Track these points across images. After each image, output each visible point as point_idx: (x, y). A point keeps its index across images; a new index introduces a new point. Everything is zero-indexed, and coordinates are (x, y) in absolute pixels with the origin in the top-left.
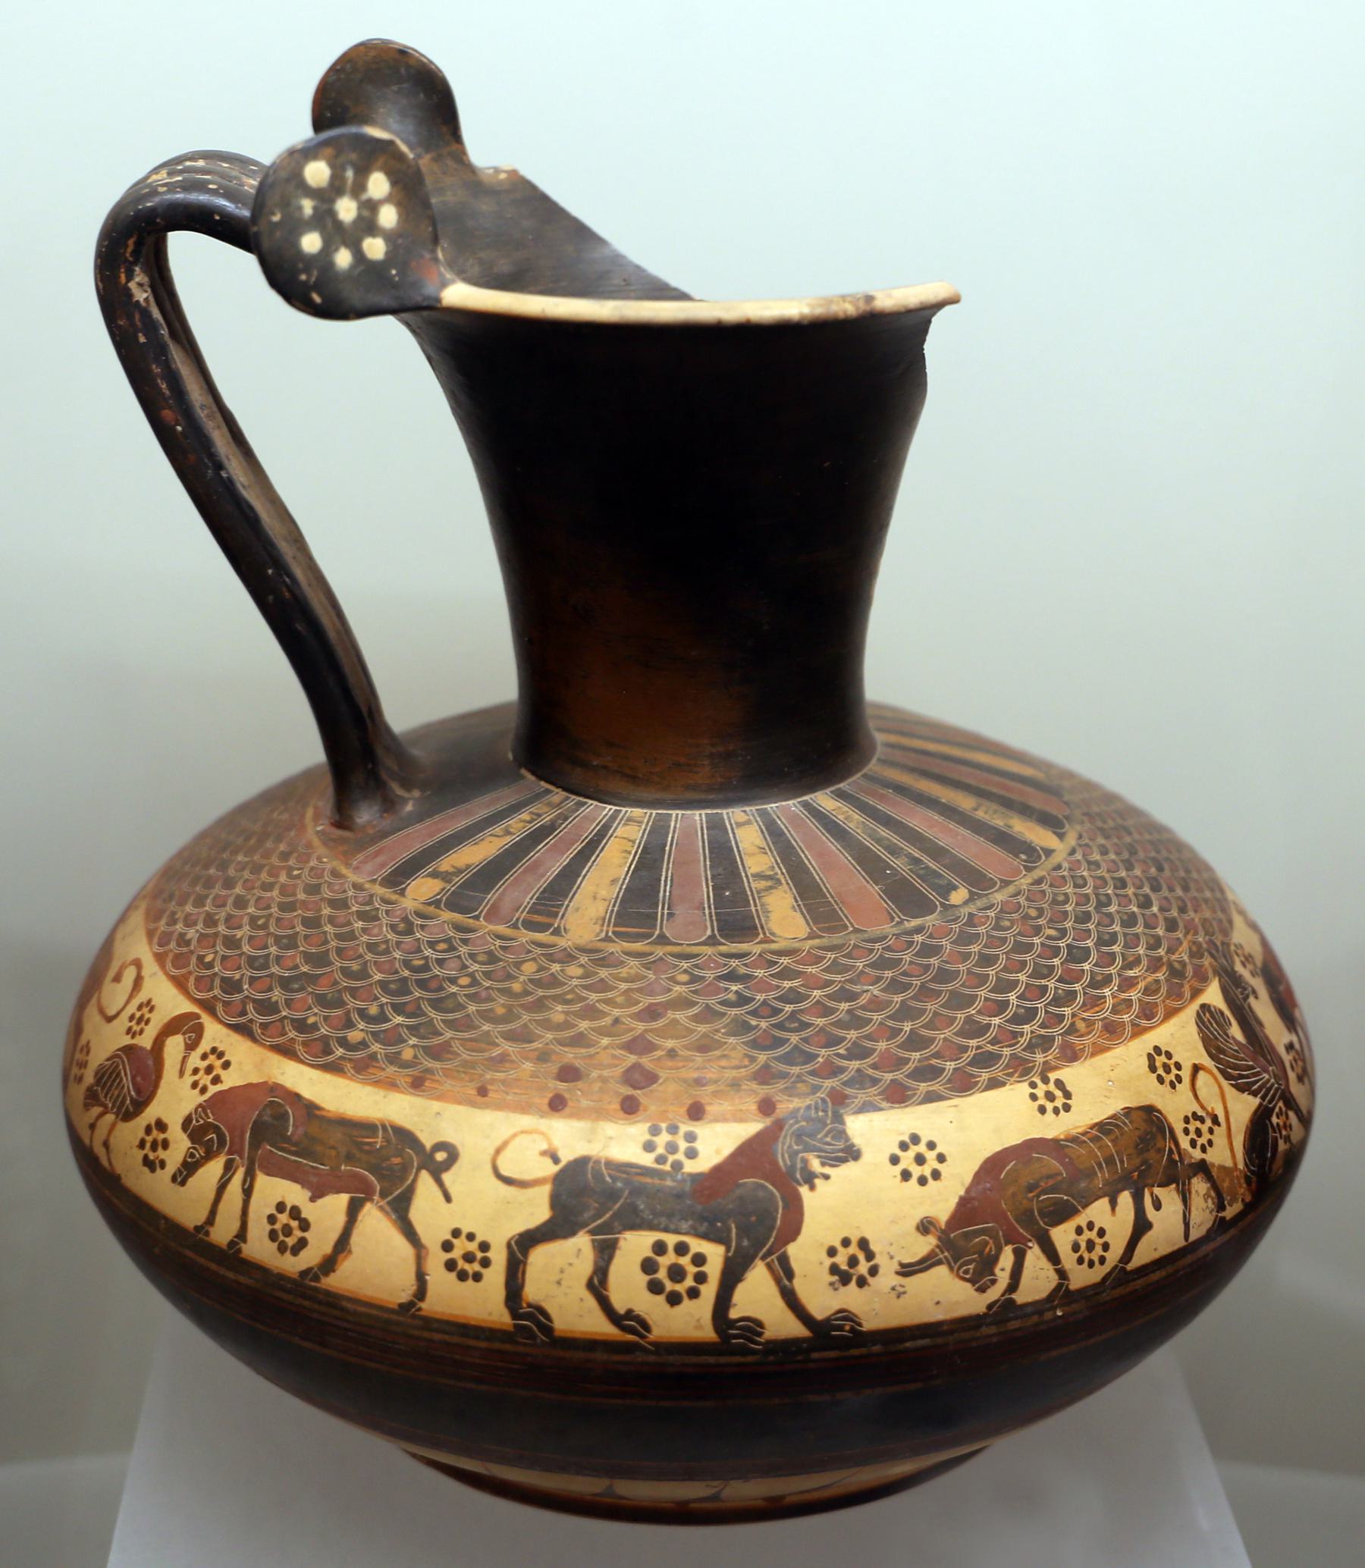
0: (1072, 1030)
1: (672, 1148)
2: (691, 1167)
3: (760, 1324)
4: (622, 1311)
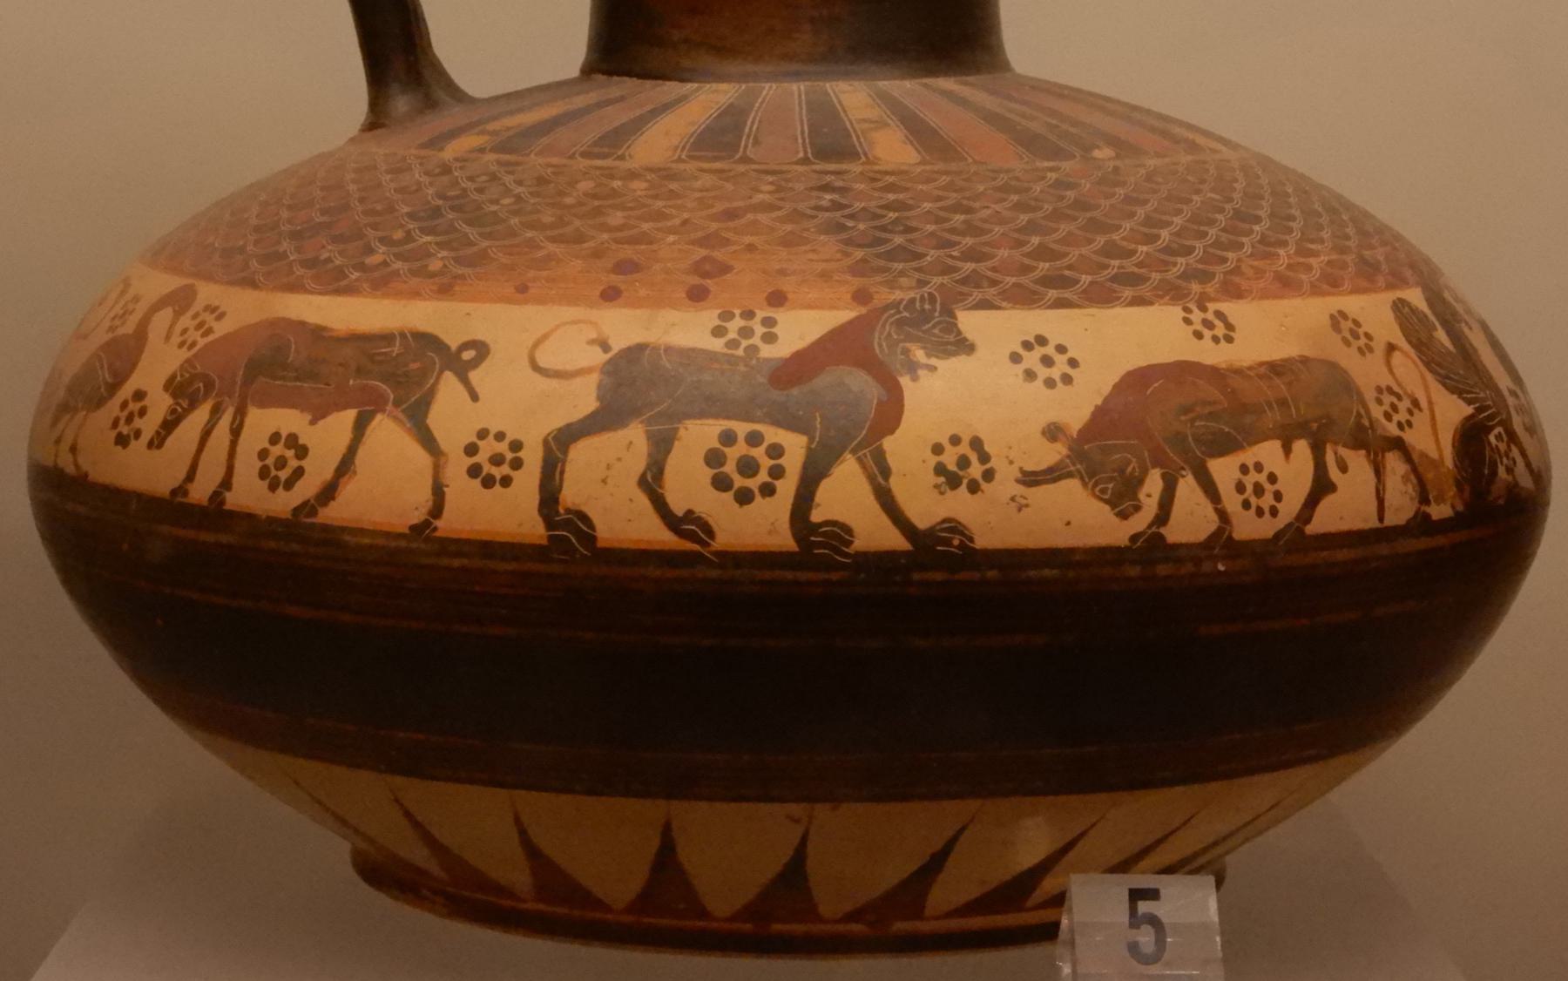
0: (1237, 271)
1: (746, 332)
2: (767, 351)
3: (848, 530)
4: (680, 513)
